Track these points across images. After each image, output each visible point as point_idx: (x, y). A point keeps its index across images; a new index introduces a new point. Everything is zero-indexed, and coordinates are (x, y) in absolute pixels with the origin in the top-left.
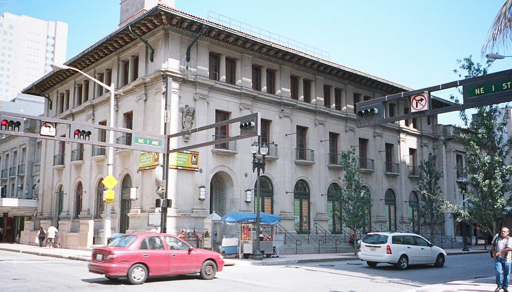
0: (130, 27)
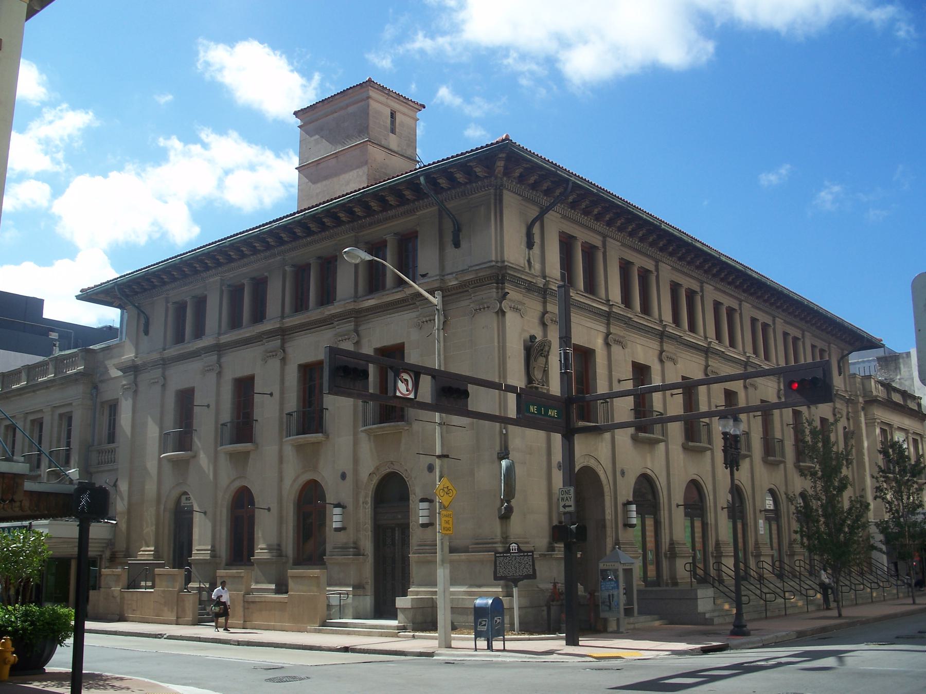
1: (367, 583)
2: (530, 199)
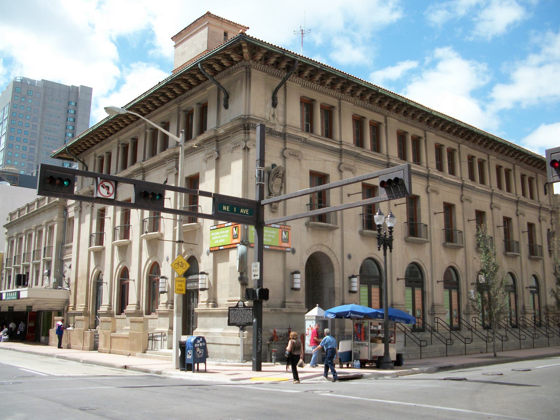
0: (199, 65)
2: (333, 96)
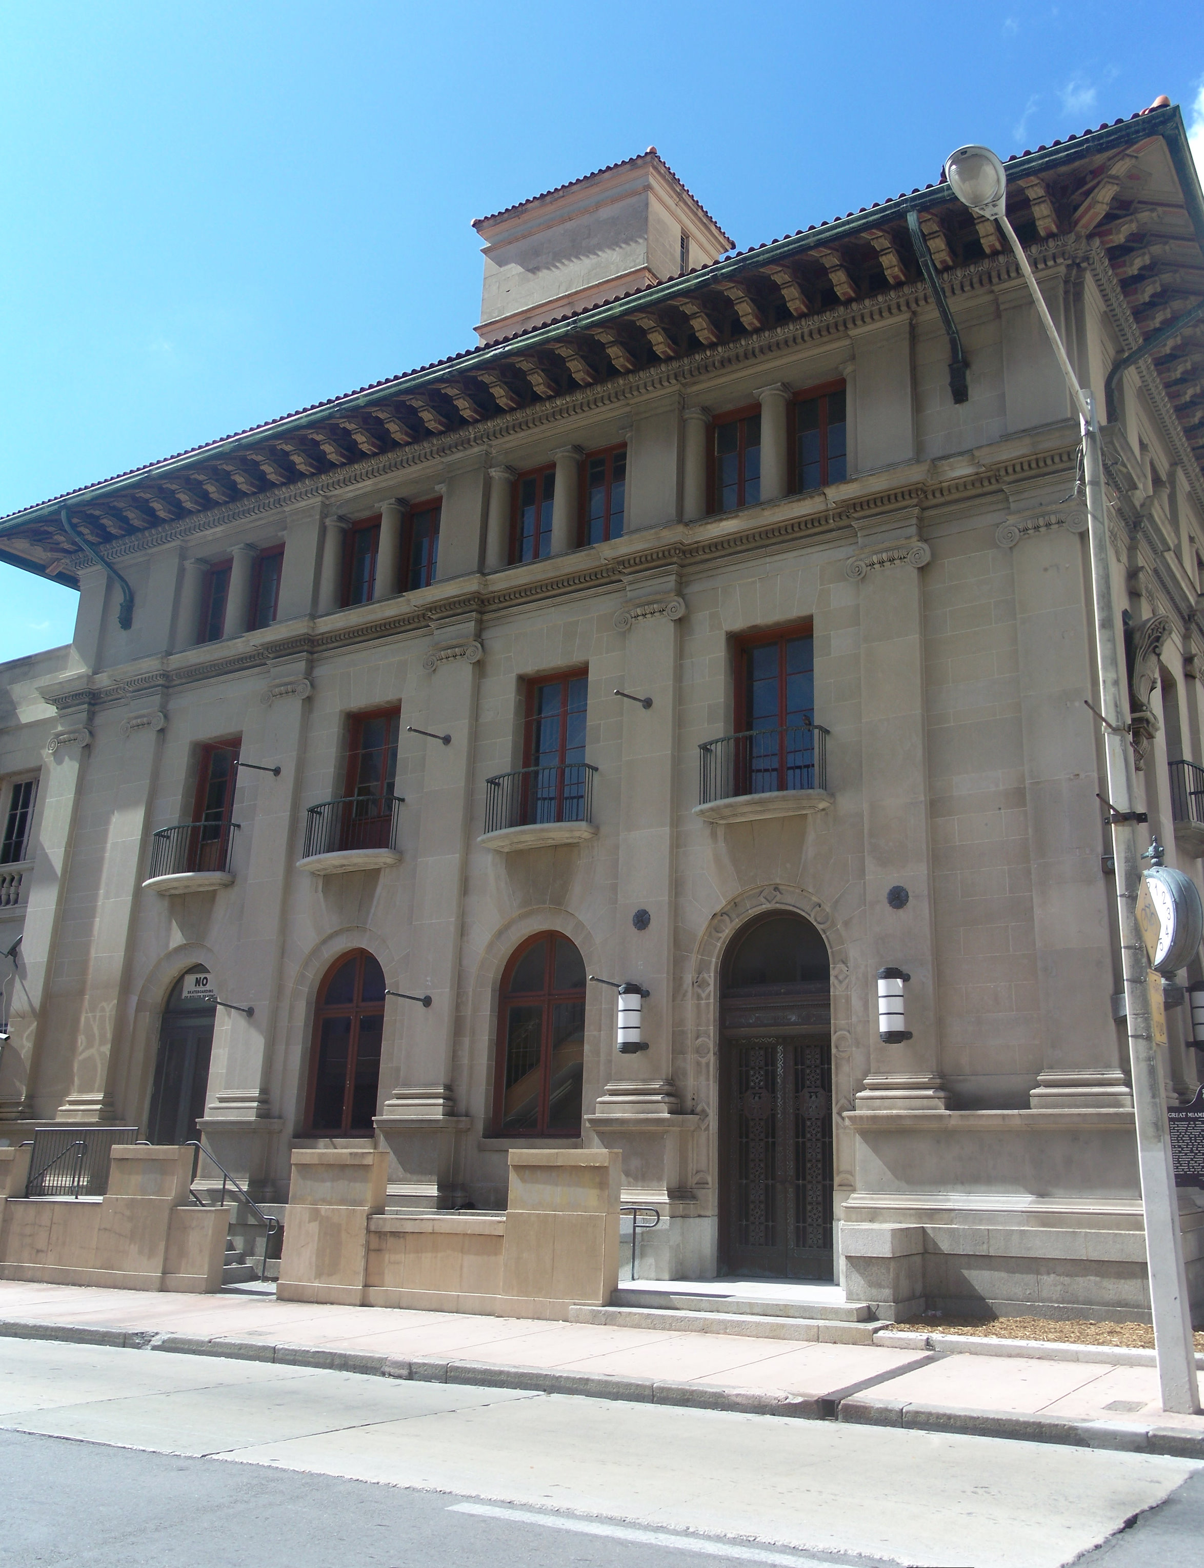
1: (702, 1184)
